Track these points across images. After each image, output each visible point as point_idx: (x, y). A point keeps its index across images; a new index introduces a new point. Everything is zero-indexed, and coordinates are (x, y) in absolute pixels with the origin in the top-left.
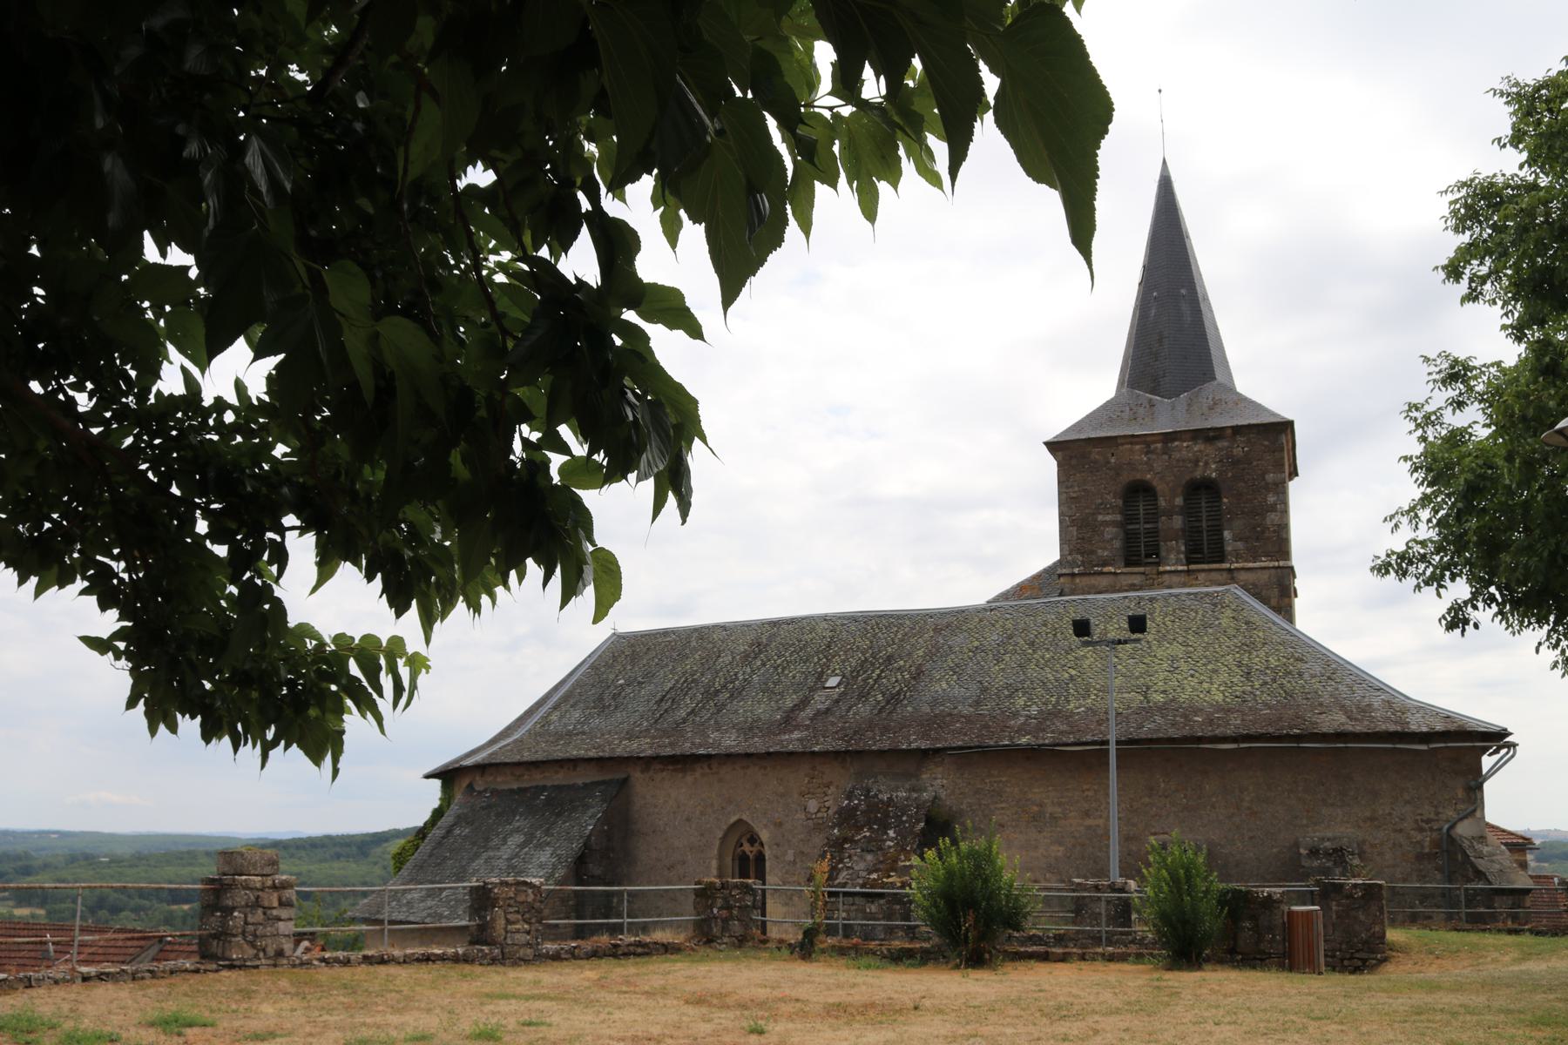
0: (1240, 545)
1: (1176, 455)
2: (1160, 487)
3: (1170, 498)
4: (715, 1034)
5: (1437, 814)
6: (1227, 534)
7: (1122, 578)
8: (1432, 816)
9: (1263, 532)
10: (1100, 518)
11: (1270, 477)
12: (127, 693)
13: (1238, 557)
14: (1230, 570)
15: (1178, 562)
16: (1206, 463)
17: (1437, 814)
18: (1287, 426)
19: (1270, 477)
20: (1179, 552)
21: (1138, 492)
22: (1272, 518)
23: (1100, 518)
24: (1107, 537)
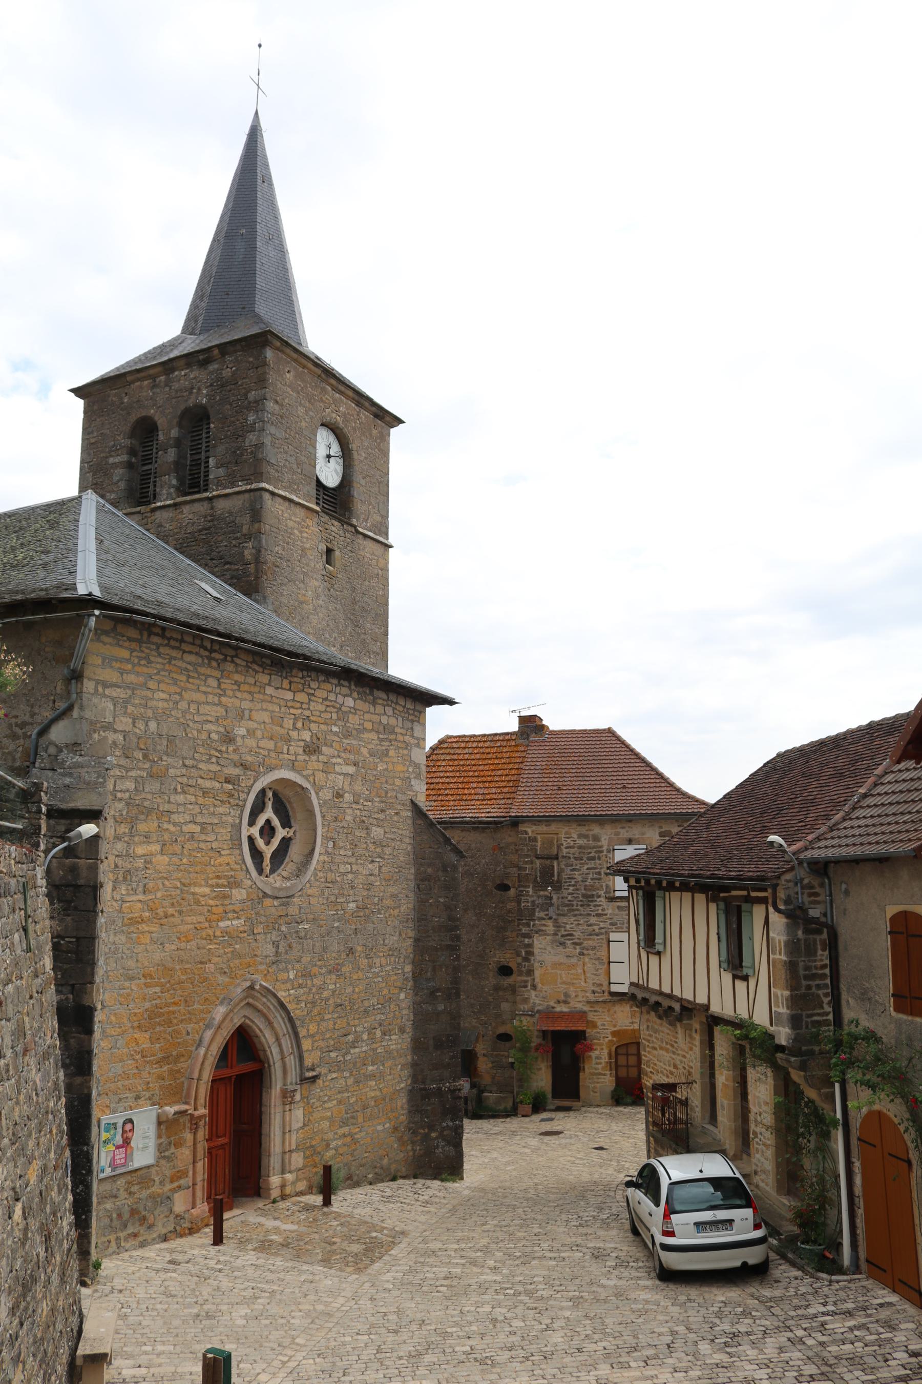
0: (221, 472)
1: (176, 386)
2: (161, 421)
3: (169, 431)
4: (878, 1379)
5: (33, 715)
6: (212, 462)
7: (186, 509)
8: (27, 718)
9: (242, 455)
10: (111, 460)
11: (252, 395)
12: (446, 706)
13: (219, 484)
14: (210, 499)
15: (169, 496)
16: (199, 389)
17: (33, 715)
18: (93, 394)
19: (252, 395)
20: (171, 486)
21: (146, 430)
22: (252, 438)
23: (111, 460)
24: (115, 478)
